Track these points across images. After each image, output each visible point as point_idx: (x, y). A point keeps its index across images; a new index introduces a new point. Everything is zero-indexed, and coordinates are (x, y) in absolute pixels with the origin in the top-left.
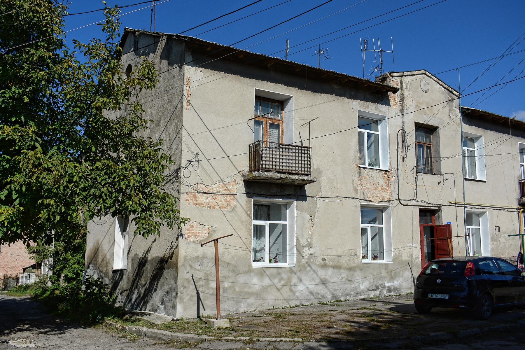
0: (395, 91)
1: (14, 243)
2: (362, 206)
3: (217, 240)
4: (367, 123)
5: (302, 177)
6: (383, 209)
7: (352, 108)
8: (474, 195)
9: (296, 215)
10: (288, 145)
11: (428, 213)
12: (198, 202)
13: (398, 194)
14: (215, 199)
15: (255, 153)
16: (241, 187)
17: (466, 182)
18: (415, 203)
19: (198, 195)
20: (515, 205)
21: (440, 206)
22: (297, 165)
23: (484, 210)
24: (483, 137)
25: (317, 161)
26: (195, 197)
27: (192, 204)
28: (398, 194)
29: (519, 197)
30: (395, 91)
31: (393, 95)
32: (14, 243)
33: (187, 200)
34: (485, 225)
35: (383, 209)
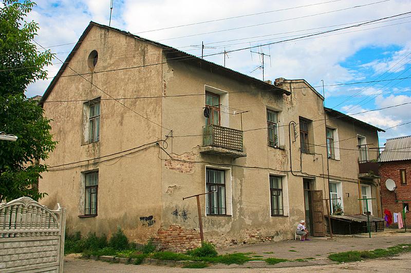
0: (288, 94)
1: (50, 128)
2: (271, 176)
3: (198, 195)
4: (272, 114)
5: (237, 153)
6: (282, 177)
7: (266, 102)
8: (335, 170)
9: (231, 180)
10: (228, 129)
11: (308, 182)
12: (173, 167)
13: (291, 167)
14: (252, 133)
15: (206, 134)
16: (197, 158)
17: (329, 160)
18: (301, 174)
19: (172, 162)
20: (356, 178)
21: (314, 177)
22: (236, 144)
23: (338, 181)
24: (337, 130)
25: (246, 142)
26: (171, 164)
27: (169, 168)
28: (291, 167)
29: (358, 173)
30: (288, 94)
31: (286, 96)
32: (50, 128)
33: (166, 165)
34: (340, 191)
35: (282, 177)
